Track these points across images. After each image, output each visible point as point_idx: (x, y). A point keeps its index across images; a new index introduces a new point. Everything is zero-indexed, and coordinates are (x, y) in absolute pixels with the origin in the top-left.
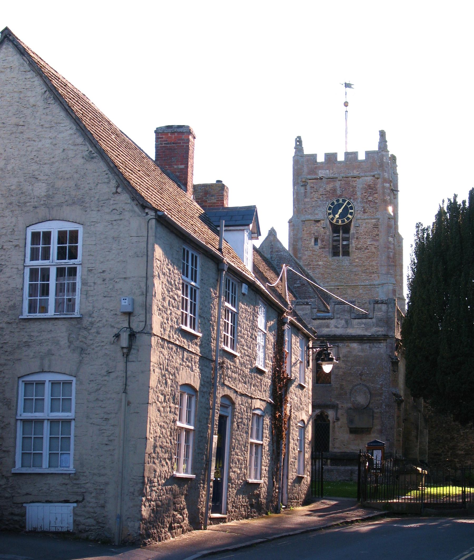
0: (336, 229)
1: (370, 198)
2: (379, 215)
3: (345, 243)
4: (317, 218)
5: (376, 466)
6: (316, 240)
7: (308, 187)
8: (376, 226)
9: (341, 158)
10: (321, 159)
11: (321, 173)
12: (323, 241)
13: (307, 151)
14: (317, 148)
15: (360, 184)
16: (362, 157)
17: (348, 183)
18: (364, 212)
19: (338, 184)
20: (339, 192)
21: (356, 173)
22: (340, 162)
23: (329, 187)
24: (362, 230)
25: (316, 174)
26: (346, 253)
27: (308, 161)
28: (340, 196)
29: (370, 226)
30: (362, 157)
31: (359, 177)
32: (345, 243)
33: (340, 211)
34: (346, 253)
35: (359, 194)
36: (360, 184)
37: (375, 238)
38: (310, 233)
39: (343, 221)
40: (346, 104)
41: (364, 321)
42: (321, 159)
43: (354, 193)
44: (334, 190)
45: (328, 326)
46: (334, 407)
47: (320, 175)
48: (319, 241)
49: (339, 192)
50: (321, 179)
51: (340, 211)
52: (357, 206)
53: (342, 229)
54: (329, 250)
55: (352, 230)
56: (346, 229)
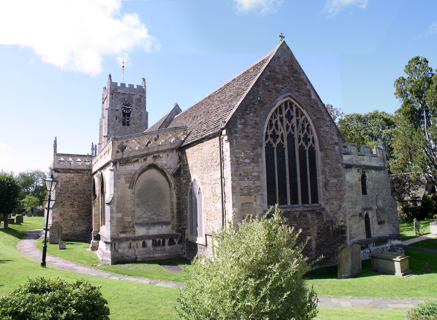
0: (124, 114)
1: (139, 104)
2: (142, 111)
3: (128, 121)
4: (117, 109)
5: (373, 244)
6: (116, 118)
7: (114, 96)
8: (141, 115)
9: (127, 86)
10: (119, 85)
11: (119, 91)
12: (119, 119)
13: (113, 81)
14: (118, 80)
15: (135, 98)
16: (135, 87)
17: (130, 97)
18: (136, 109)
19: (126, 96)
20: (126, 100)
21: (133, 93)
22: (127, 88)
23: (122, 97)
24: (135, 116)
25: (117, 91)
26: (128, 125)
27: (114, 85)
28: (127, 101)
29: (138, 115)
30: (135, 87)
31: (134, 95)
32: (128, 121)
33: (127, 107)
34: (128, 125)
35: (134, 101)
36: (135, 98)
37: (140, 120)
38: (114, 115)
39: (128, 112)
40: (123, 67)
41: (376, 158)
42: (119, 85)
43: (132, 101)
44: (124, 99)
45: (364, 160)
46: (371, 209)
47: (118, 92)
48: (118, 119)
49: (126, 100)
50: (119, 93)
51: (127, 107)
52: (134, 106)
53: (126, 115)
54: (121, 122)
55: (131, 116)
56: (129, 115)
